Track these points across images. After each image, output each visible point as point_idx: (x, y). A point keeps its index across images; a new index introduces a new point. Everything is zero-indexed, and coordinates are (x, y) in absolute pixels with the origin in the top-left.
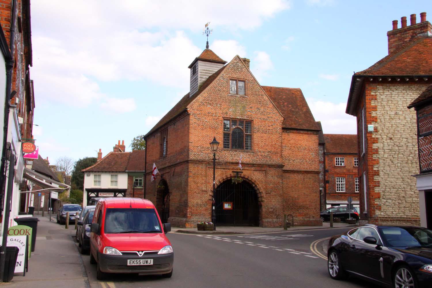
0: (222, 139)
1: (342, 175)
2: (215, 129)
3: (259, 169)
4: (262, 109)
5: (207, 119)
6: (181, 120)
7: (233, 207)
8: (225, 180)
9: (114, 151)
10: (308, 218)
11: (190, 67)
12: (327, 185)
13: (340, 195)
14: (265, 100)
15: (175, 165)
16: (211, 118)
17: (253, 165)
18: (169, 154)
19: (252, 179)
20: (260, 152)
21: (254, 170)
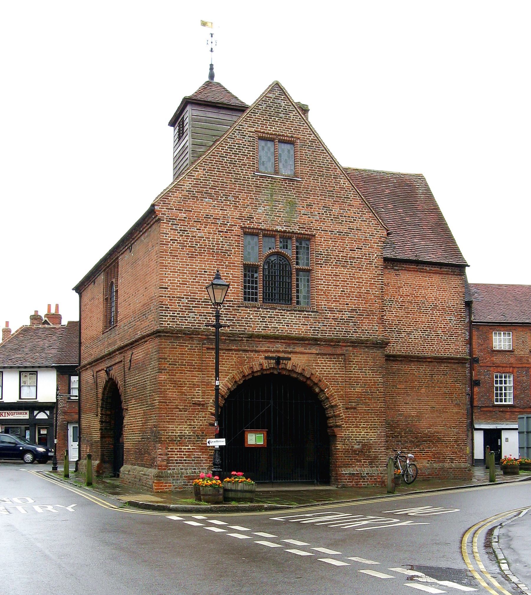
0: (241, 279)
1: (507, 369)
2: (222, 254)
3: (330, 350)
4: (336, 210)
5: (204, 232)
6: (142, 238)
7: (268, 440)
8: (247, 378)
9: (33, 323)
10: (440, 462)
11: (172, 123)
12: (476, 389)
13: (502, 411)
14: (342, 188)
15: (132, 343)
16: (211, 228)
17: (315, 341)
18: (121, 320)
19: (312, 374)
20: (331, 310)
21: (318, 354)
